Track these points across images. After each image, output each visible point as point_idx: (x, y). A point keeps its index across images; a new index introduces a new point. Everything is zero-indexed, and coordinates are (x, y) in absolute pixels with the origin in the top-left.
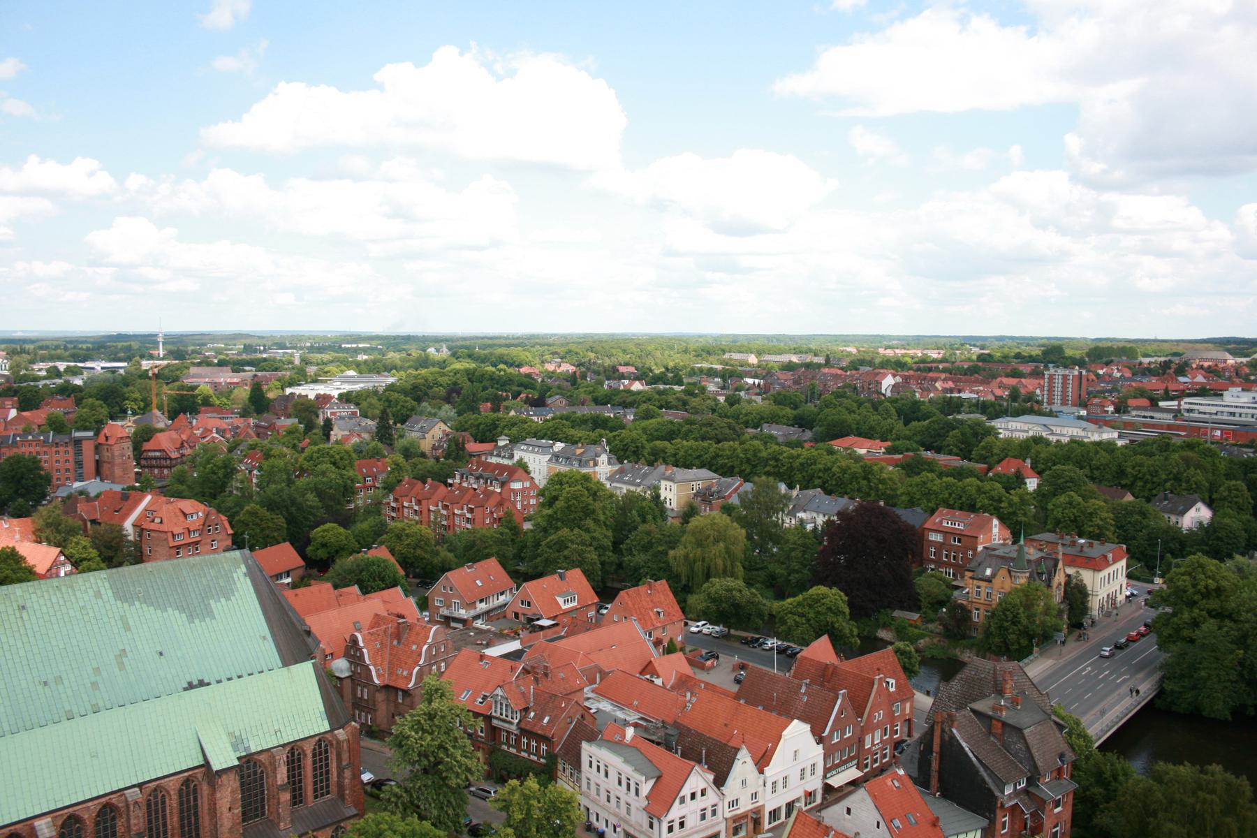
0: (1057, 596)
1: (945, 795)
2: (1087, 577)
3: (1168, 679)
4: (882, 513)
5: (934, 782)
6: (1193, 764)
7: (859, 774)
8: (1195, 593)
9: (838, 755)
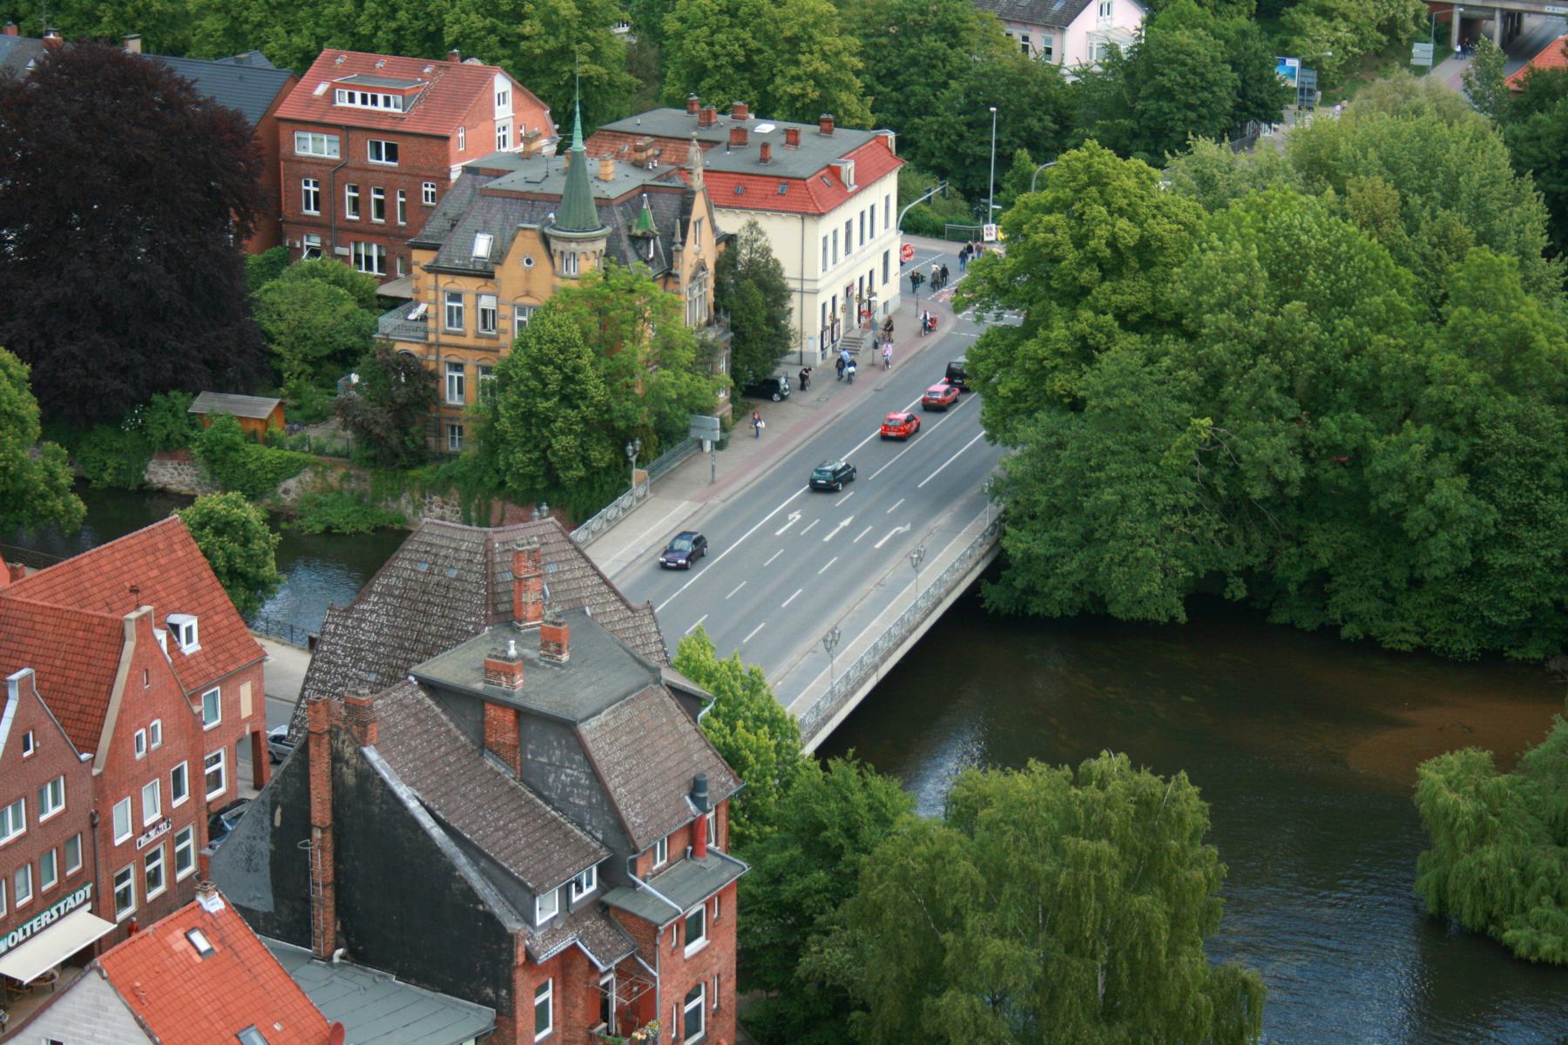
0: (694, 304)
1: (361, 955)
2: (782, 238)
3: (1017, 522)
4: (133, 75)
5: (324, 918)
6: (1054, 763)
7: (102, 928)
8: (1081, 266)
9: (24, 879)
